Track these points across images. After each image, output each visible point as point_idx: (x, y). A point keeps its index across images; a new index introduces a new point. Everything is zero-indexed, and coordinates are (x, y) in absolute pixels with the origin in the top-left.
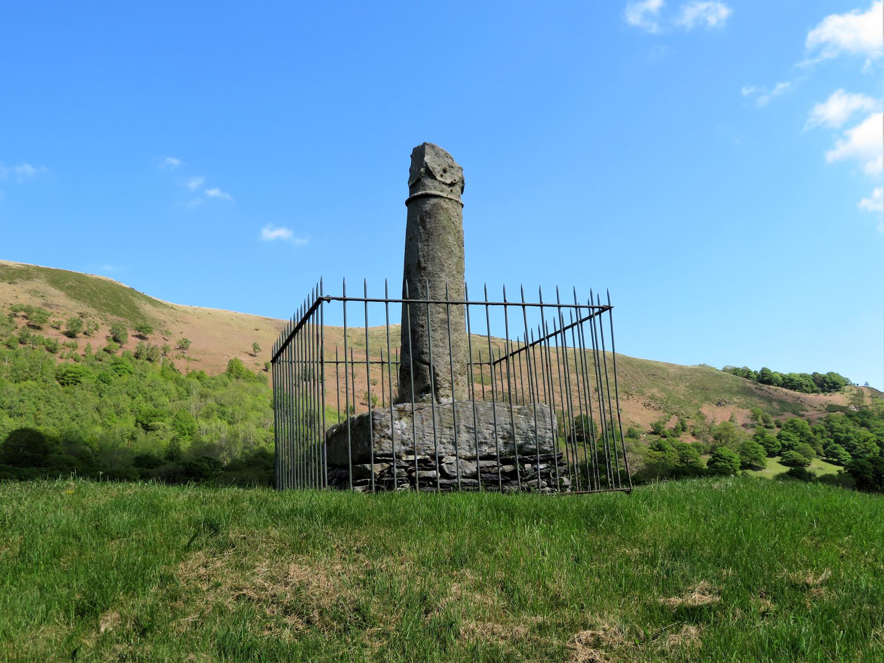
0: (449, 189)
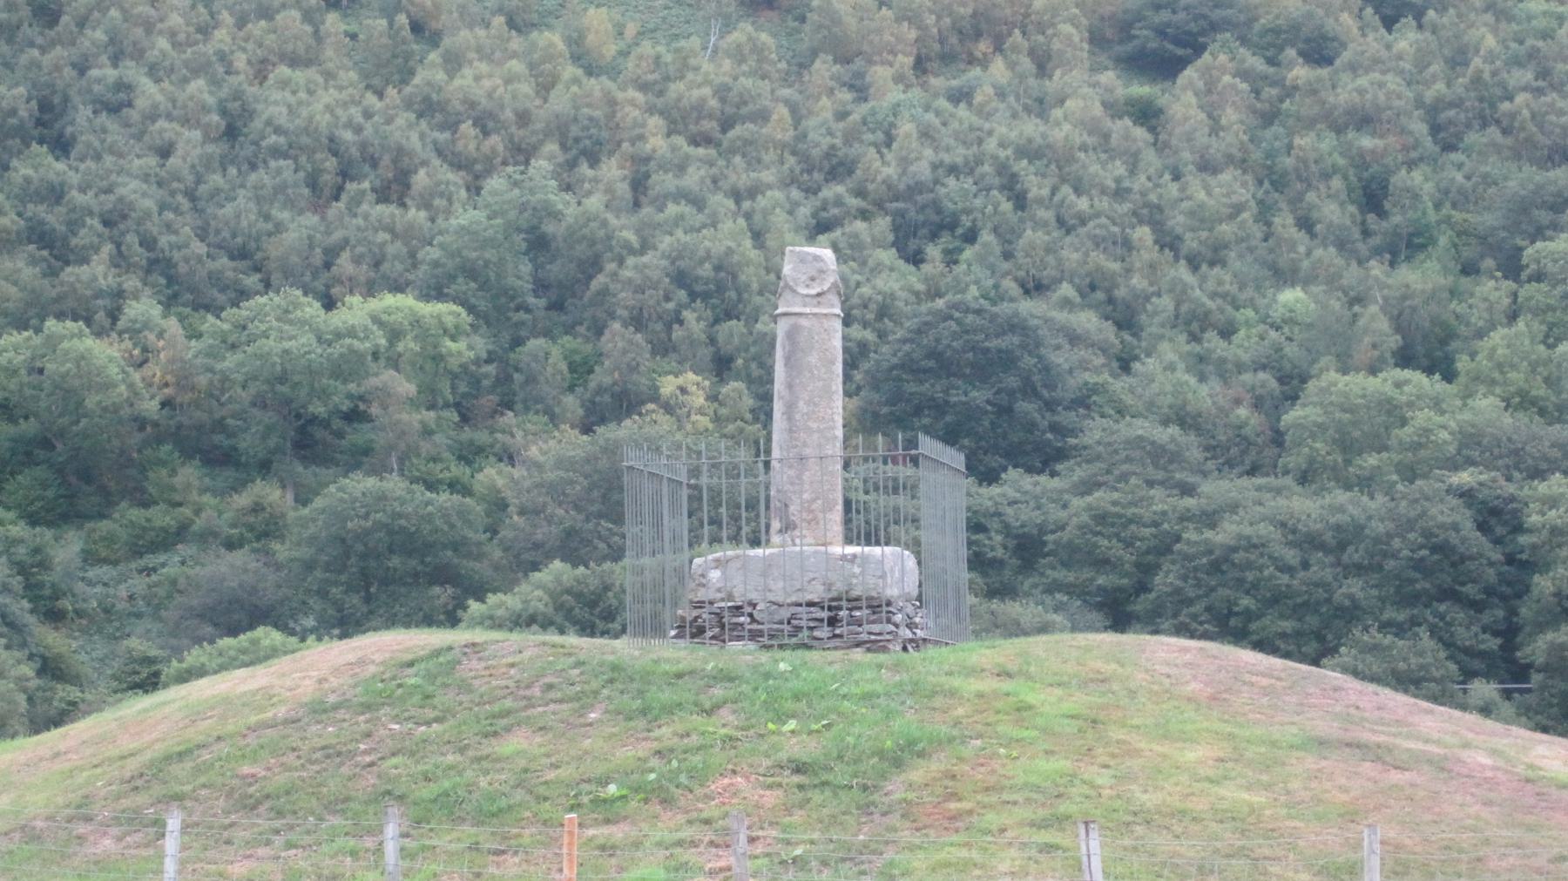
0: (815, 301)
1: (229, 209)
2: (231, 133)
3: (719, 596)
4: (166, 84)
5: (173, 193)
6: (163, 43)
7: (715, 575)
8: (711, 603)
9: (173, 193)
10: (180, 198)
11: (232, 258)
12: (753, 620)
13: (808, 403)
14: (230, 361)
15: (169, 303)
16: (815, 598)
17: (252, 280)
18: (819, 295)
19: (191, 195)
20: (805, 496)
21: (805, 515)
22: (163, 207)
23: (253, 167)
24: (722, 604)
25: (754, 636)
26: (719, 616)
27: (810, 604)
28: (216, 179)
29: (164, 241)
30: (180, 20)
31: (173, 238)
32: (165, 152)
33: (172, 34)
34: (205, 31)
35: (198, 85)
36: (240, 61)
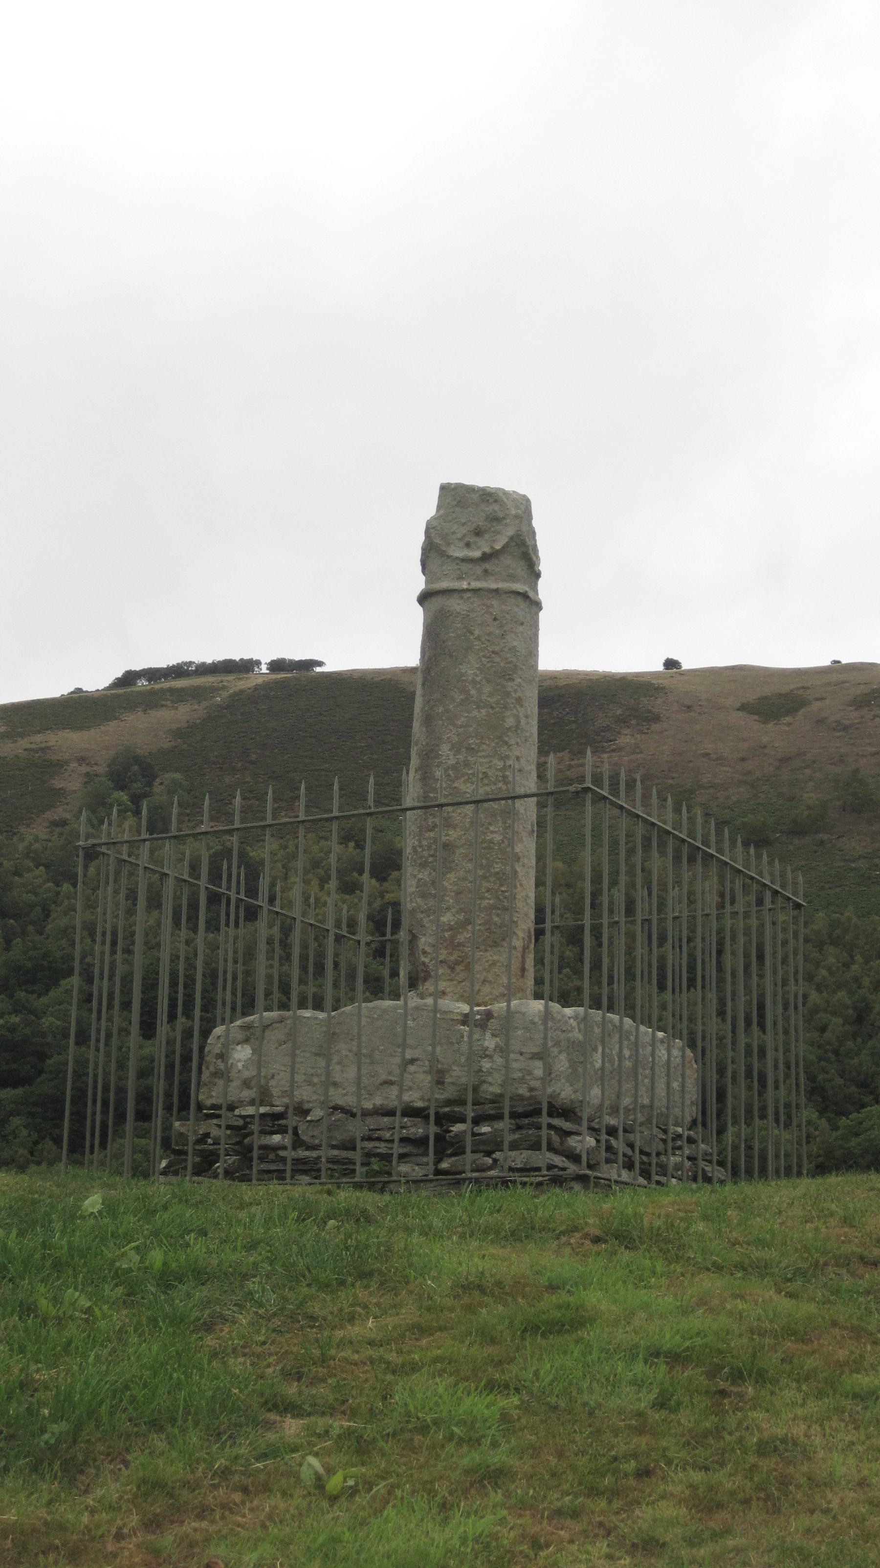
0: (478, 570)
1: (856, 1061)
2: (860, 1019)
3: (247, 1094)
4: (825, 995)
5: (826, 1052)
6: (824, 972)
7: (242, 1054)
8: (231, 1108)
9: (826, 1052)
10: (830, 1054)
11: (858, 1086)
12: (298, 1143)
13: (456, 748)
14: (854, 1142)
15: (822, 1112)
16: (414, 1098)
17: (867, 1099)
18: (485, 557)
19: (836, 1053)
20: (446, 918)
21: (443, 954)
22: (820, 1059)
23: (871, 1037)
24: (250, 1110)
25: (307, 1168)
26: (241, 1130)
27: (411, 1112)
28: (850, 1044)
29: (821, 1077)
30: (834, 960)
31: (826, 1076)
32: (823, 1029)
33: (829, 969)
34: (847, 966)
35: (842, 994)
36: (866, 981)
